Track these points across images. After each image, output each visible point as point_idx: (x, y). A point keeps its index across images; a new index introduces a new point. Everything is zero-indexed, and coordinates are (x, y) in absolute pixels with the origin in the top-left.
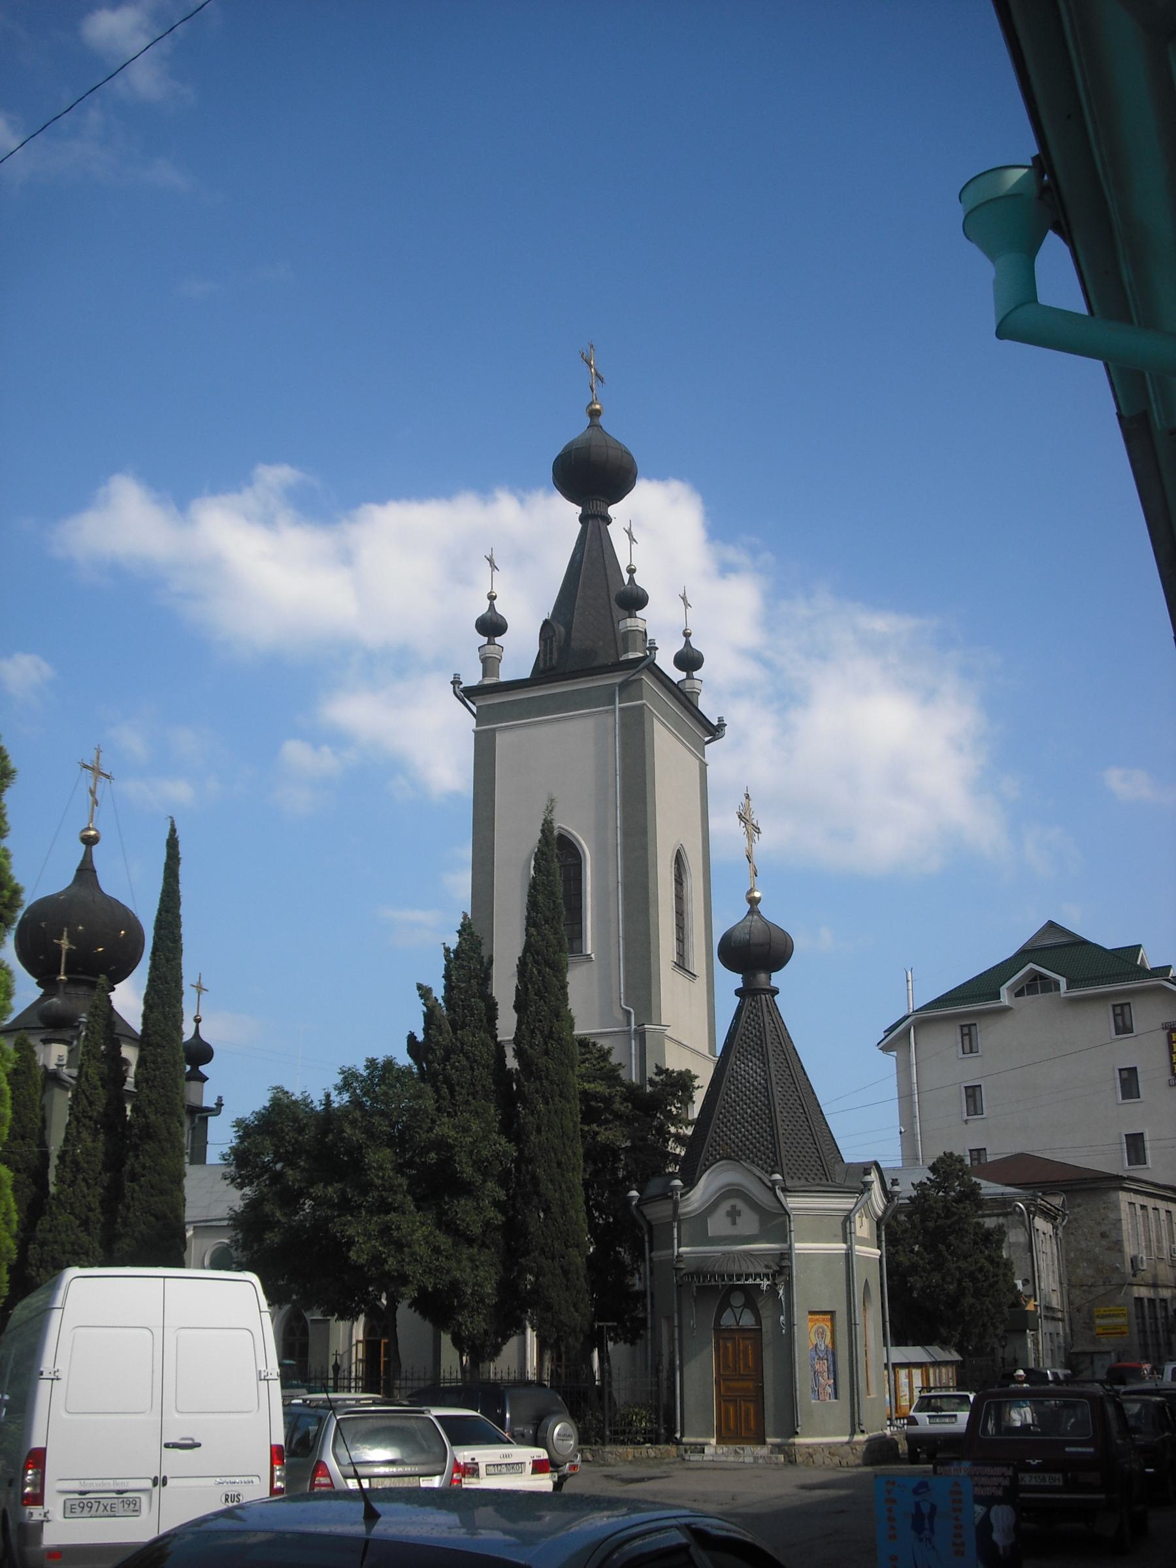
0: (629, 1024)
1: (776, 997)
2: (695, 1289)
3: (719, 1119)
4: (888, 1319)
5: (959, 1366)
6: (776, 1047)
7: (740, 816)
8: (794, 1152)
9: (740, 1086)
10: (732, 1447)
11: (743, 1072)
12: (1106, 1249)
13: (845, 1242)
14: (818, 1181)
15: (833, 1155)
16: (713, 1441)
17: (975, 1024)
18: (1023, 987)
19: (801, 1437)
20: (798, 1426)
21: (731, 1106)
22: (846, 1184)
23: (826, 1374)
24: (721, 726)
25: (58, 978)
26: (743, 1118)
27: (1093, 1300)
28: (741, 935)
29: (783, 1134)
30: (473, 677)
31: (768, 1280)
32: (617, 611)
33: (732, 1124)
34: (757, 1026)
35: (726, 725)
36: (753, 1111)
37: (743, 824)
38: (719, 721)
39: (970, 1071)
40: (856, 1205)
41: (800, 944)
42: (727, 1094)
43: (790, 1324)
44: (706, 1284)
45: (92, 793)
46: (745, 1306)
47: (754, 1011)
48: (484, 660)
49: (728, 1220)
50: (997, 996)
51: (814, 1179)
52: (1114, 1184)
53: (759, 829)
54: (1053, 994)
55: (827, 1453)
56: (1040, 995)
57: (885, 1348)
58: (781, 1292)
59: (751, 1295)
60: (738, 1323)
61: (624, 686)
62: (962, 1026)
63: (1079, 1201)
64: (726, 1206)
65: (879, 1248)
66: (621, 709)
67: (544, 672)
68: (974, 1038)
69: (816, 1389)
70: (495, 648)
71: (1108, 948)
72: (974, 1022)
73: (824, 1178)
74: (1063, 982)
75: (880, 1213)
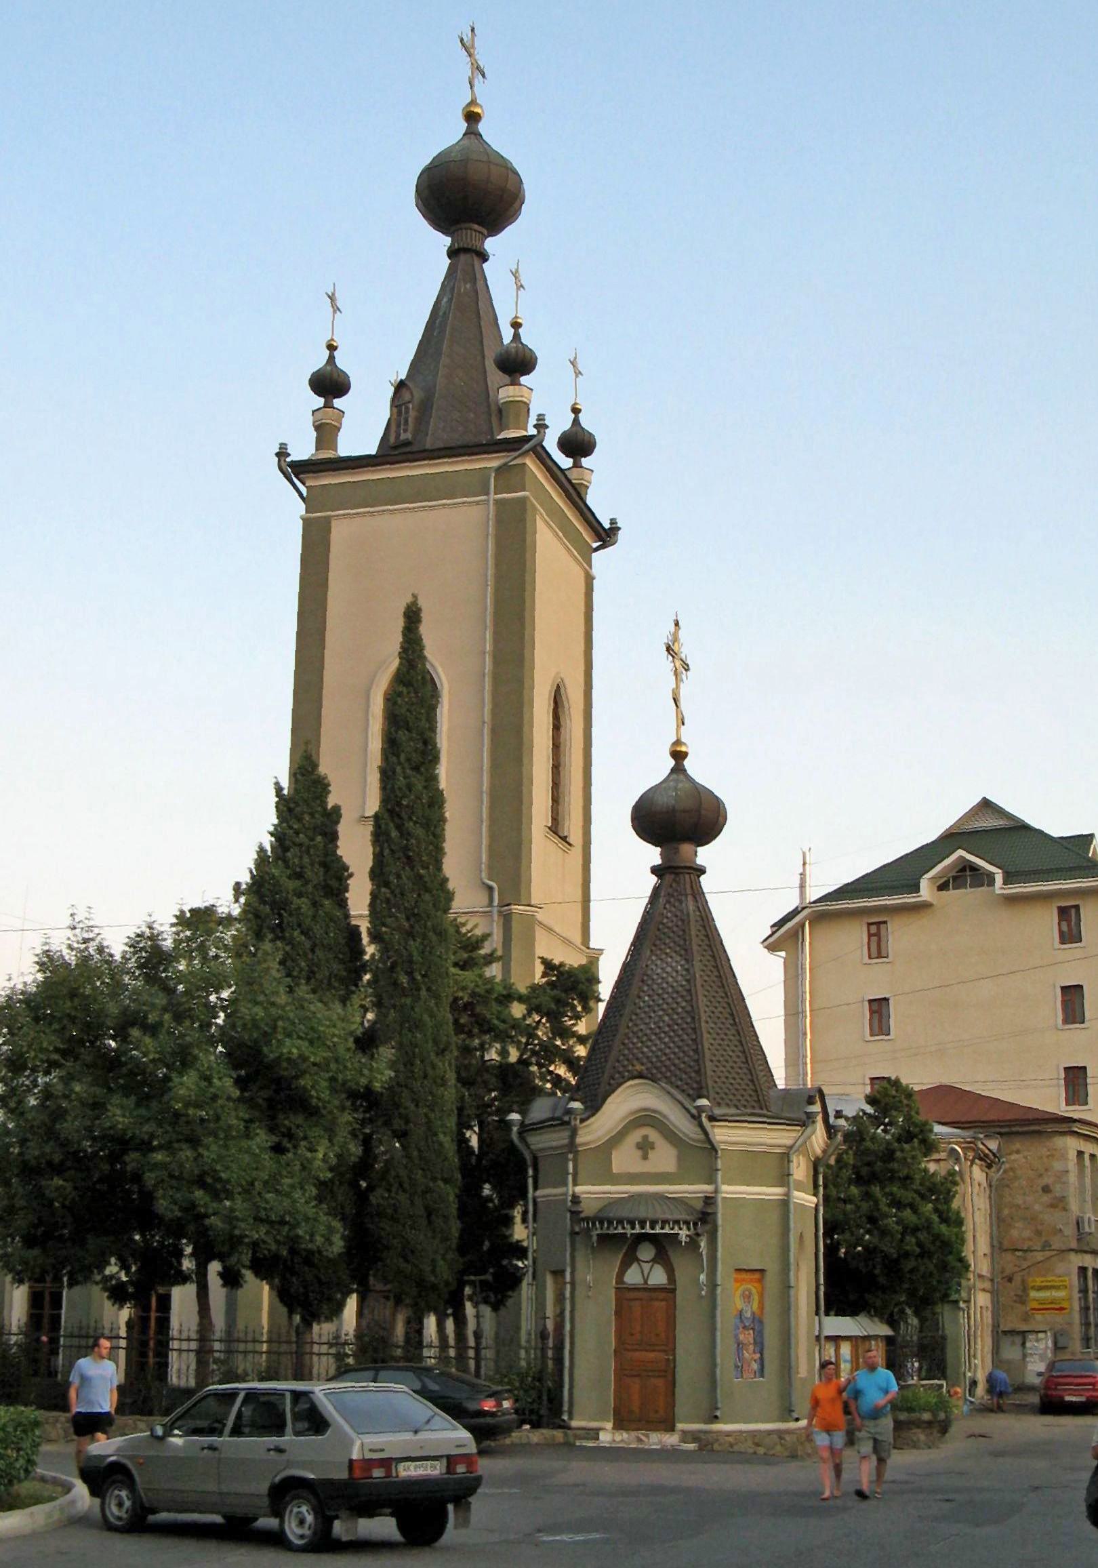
1: (702, 878)
2: (595, 1238)
4: (822, 1281)
10: (634, 1434)
12: (1048, 1206)
14: (749, 1111)
16: (609, 1425)
17: (885, 922)
23: (751, 1347)
24: (614, 530)
27: (1029, 1267)
28: (664, 800)
30: (304, 448)
31: (689, 1229)
32: (495, 376)
37: (670, 658)
38: (611, 524)
44: (611, 1231)
48: (319, 428)
49: (639, 1153)
50: (916, 889)
52: (1063, 1127)
53: (688, 665)
54: (985, 889)
56: (969, 890)
57: (817, 1318)
58: (703, 1244)
59: (663, 1246)
60: (646, 1282)
62: (869, 924)
63: (1018, 1146)
64: (636, 1136)
65: (815, 1195)
66: (497, 502)
68: (883, 939)
70: (333, 413)
71: (1055, 832)
72: (885, 919)
74: (999, 879)
75: (819, 1152)
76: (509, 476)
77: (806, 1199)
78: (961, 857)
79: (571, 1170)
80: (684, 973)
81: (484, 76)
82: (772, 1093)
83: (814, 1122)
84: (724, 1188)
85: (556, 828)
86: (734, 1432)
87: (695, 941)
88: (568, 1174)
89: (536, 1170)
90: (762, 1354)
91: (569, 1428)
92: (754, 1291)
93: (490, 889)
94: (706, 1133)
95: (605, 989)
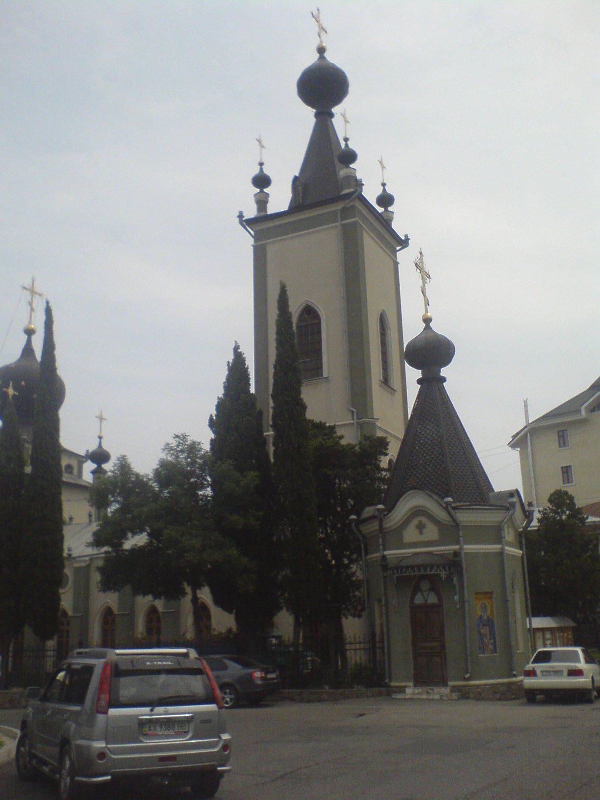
5: (574, 630)
7: (416, 264)
10: (427, 689)
16: (411, 684)
18: (595, 407)
23: (488, 636)
24: (407, 239)
30: (251, 212)
31: (446, 570)
32: (338, 164)
39: (564, 458)
45: (31, 304)
49: (417, 531)
53: (430, 276)
58: (455, 579)
61: (344, 210)
64: (415, 522)
65: (521, 549)
67: (296, 206)
69: (482, 647)
78: (586, 408)
81: (326, 32)
82: (490, 494)
84: (465, 547)
85: (386, 381)
86: (481, 685)
88: (380, 545)
90: (494, 639)
91: (390, 686)
92: (487, 605)
93: (353, 412)
94: (451, 516)
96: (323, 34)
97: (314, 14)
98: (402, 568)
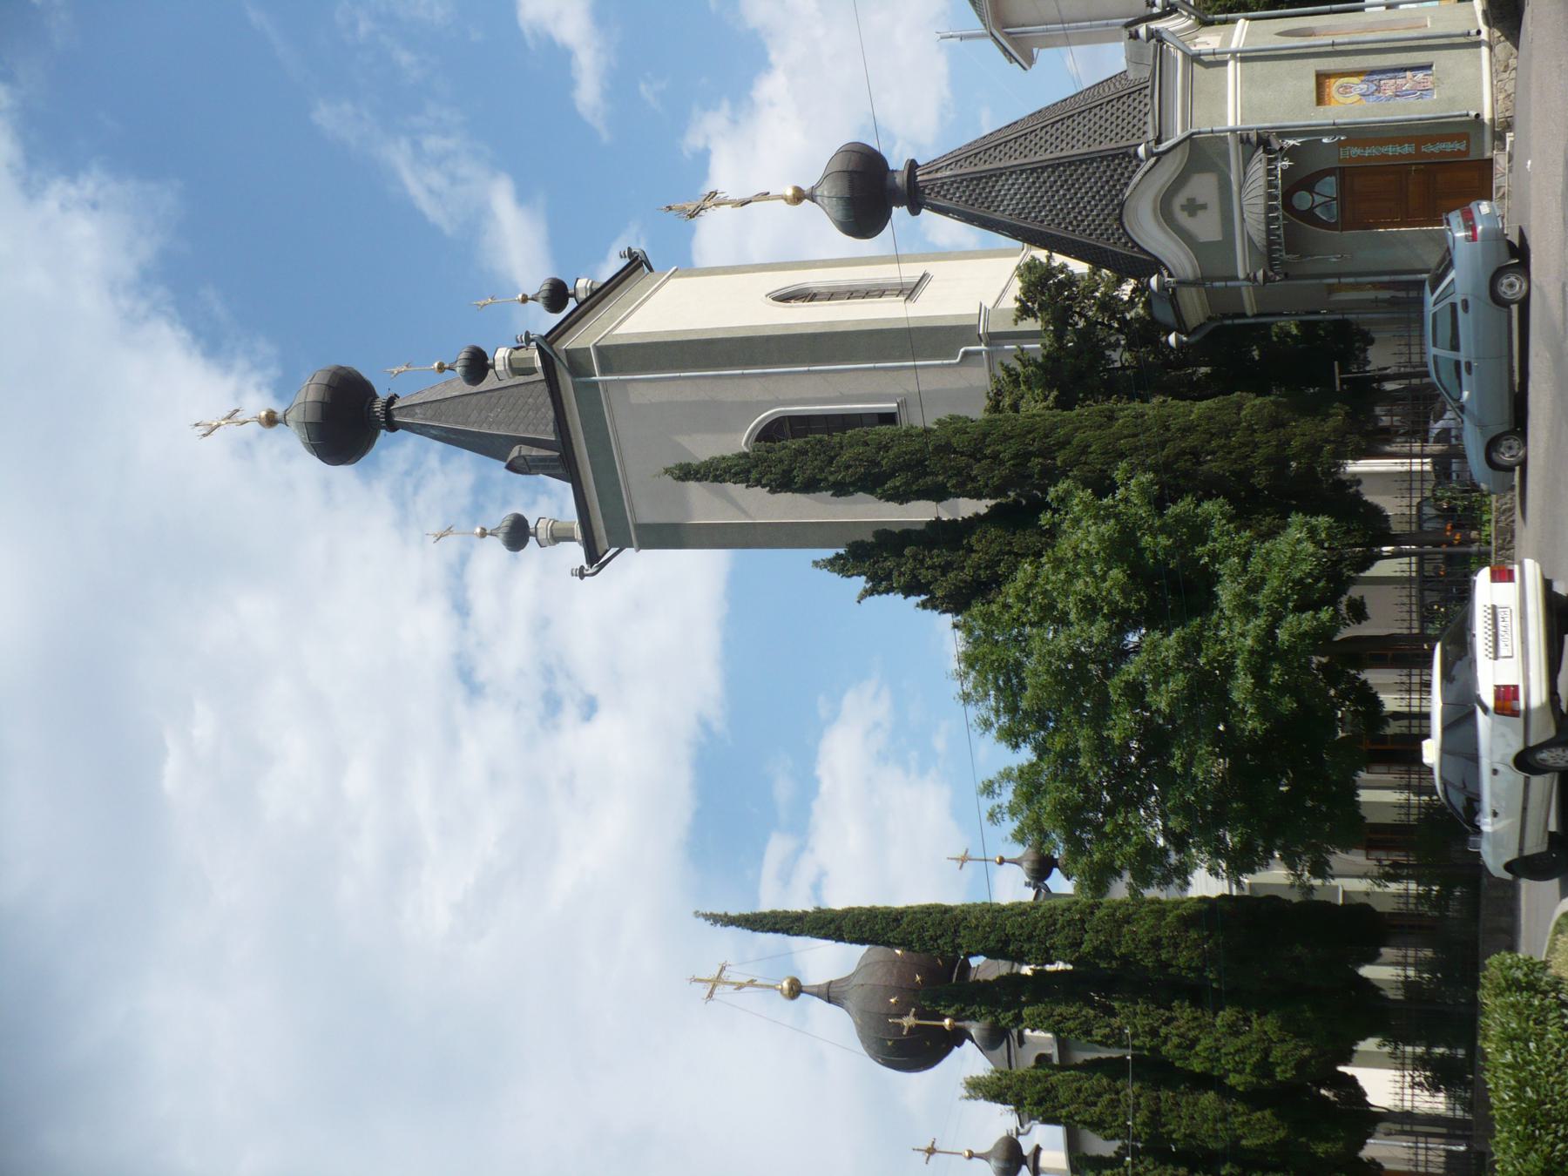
0: (979, 353)
1: (920, 163)
3: (1074, 231)
6: (980, 159)
8: (1112, 131)
9: (1031, 205)
11: (1014, 202)
13: (1225, 63)
15: (1117, 84)
19: (1483, 111)
20: (1467, 115)
21: (1057, 215)
22: (1151, 62)
23: (1399, 81)
25: (947, 1028)
26: (1071, 199)
29: (1089, 146)
30: (574, 553)
31: (1276, 159)
32: (489, 382)
33: (1080, 213)
34: (955, 185)
35: (629, 249)
36: (1062, 186)
40: (1178, 48)
41: (911, 158)
42: (1042, 221)
43: (1335, 130)
45: (740, 986)
46: (1311, 191)
47: (936, 190)
49: (1200, 213)
51: (1146, 105)
55: (1505, 75)
57: (1367, 10)
58: (1291, 142)
60: (1334, 199)
64: (1182, 218)
65: (1234, 21)
67: (565, 467)
73: (1144, 92)
76: (577, 363)
77: (1241, 33)
79: (1223, 284)
80: (1014, 176)
83: (1157, 31)
87: (982, 167)
89: (1225, 316)
95: (1041, 254)
96: (240, 417)
97: (205, 432)
98: (1270, 243)
